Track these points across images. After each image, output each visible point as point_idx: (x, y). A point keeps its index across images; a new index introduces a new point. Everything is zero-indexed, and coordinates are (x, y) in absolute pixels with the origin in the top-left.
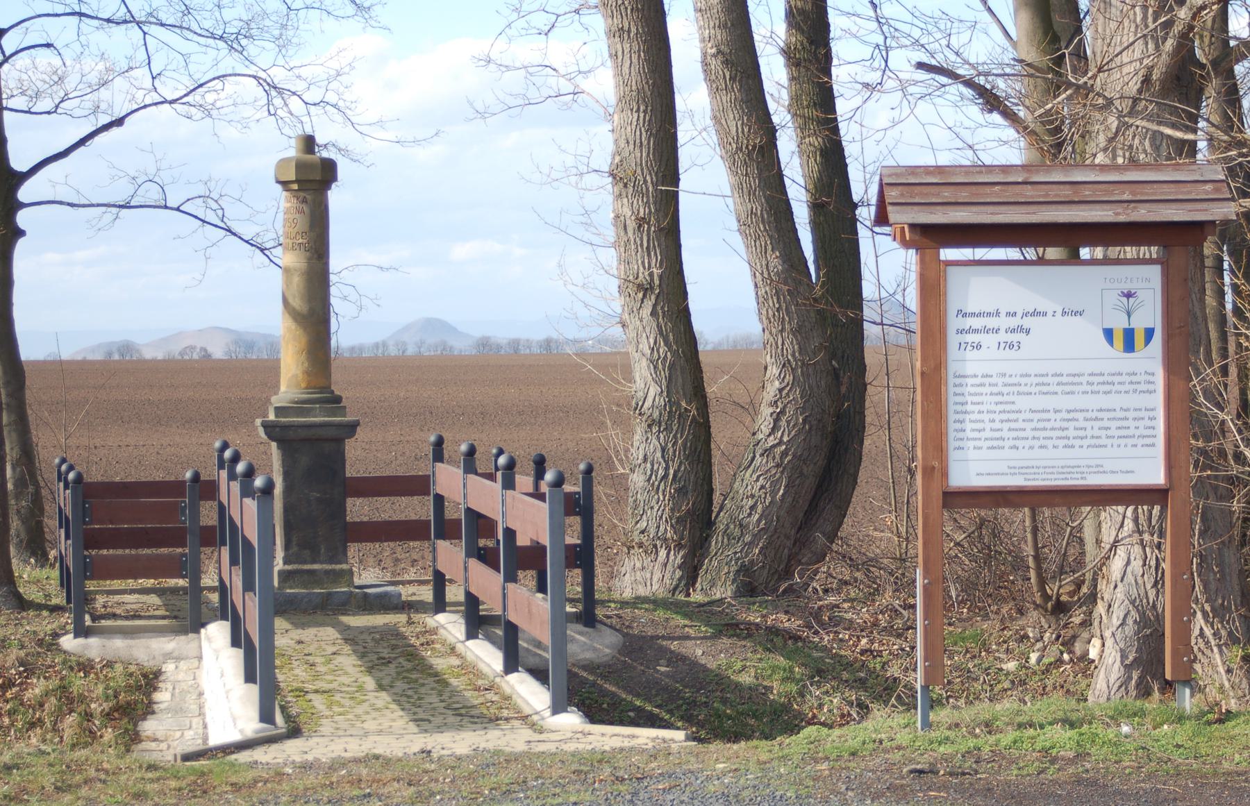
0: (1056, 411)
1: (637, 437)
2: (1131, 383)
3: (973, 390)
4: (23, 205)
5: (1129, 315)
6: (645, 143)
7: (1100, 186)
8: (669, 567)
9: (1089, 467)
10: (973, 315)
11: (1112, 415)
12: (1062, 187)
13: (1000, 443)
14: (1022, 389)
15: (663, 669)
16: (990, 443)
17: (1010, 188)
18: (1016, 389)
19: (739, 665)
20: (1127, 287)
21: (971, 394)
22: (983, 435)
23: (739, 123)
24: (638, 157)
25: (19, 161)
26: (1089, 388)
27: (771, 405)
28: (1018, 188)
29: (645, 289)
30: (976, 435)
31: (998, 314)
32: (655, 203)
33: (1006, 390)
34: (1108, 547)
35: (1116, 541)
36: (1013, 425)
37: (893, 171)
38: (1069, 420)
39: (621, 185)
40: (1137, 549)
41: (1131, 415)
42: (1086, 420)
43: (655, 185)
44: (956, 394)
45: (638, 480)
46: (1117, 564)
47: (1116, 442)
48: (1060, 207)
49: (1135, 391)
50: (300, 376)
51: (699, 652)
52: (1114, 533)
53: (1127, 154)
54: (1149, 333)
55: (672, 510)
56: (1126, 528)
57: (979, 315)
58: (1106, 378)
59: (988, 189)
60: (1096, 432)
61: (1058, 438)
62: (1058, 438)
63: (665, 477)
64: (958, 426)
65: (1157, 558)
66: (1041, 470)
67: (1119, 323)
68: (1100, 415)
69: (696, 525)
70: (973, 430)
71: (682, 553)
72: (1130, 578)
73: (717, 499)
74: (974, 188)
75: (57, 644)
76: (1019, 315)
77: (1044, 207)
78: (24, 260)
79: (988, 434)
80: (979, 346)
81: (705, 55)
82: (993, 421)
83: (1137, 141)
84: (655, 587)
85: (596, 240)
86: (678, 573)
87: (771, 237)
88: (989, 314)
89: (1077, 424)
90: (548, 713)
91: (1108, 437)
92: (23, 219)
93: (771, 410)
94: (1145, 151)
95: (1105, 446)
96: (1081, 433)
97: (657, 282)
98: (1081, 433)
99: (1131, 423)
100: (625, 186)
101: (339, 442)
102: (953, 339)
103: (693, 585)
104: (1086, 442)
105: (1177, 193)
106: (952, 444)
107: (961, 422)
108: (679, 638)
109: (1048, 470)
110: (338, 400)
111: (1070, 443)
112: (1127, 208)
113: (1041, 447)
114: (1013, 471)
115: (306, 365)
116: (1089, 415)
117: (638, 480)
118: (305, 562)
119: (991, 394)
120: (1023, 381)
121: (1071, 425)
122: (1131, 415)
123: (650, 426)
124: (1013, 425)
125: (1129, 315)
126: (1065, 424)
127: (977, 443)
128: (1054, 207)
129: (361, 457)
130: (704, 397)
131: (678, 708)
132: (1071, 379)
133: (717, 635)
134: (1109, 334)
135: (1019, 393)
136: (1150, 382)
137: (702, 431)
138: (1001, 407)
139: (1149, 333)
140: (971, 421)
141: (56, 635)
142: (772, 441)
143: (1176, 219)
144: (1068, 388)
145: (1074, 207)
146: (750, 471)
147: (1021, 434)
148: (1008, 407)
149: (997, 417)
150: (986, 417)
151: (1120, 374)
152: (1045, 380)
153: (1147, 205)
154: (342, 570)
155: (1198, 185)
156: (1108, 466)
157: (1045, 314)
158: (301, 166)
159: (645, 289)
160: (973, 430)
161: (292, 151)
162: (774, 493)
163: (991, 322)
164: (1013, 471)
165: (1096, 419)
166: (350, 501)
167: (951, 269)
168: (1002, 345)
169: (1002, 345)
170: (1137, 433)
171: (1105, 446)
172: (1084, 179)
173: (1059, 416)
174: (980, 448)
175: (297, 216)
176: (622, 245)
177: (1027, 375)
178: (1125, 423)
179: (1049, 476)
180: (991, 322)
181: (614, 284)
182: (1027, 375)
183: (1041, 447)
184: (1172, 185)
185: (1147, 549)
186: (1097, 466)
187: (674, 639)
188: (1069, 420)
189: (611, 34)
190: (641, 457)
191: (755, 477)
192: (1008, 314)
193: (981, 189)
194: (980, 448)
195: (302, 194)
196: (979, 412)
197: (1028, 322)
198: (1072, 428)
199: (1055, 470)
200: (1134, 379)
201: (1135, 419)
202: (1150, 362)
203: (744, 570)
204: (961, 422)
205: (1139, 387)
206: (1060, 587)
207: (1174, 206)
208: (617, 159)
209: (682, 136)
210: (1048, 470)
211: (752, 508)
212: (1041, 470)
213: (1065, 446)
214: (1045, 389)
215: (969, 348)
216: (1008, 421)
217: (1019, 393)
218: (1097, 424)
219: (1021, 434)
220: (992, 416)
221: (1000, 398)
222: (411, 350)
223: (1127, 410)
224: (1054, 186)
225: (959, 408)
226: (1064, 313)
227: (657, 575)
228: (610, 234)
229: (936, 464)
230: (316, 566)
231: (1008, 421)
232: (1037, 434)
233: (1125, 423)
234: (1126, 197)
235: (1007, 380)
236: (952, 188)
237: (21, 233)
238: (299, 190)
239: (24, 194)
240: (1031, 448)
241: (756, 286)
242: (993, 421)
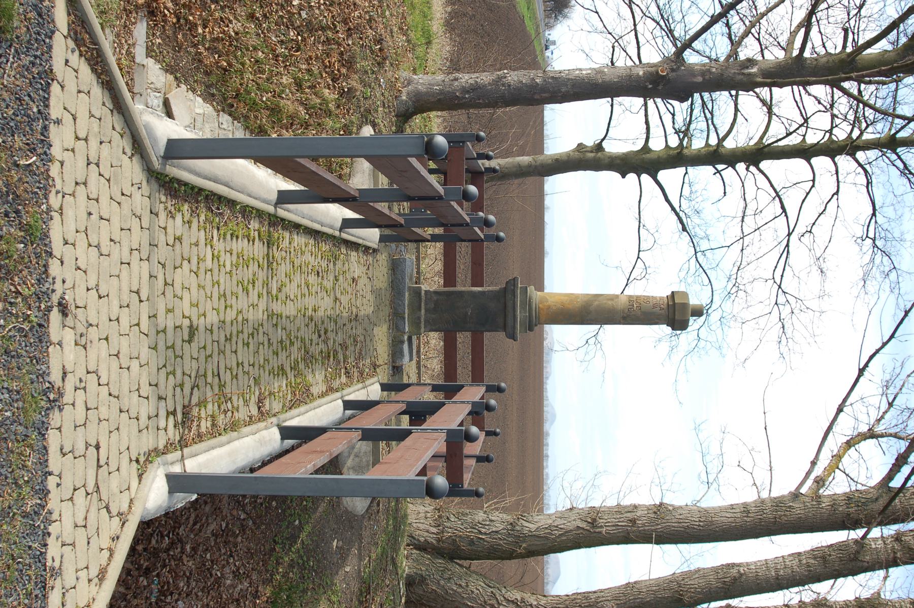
1: (505, 516)
6: (680, 525)
8: (426, 534)
15: (335, 544)
19: (334, 599)
24: (672, 522)
27: (522, 599)
29: (593, 523)
32: (644, 530)
39: (655, 510)
43: (655, 530)
45: (480, 516)
51: (348, 569)
55: (460, 536)
63: (480, 533)
69: (450, 551)
71: (434, 542)
73: (466, 563)
75: (367, 124)
81: (739, 565)
84: (414, 525)
85: (622, 494)
86: (422, 539)
87: (625, 603)
90: (177, 469)
92: (632, 176)
93: (519, 599)
97: (598, 530)
100: (655, 513)
101: (504, 328)
103: (415, 548)
108: (360, 554)
110: (531, 329)
117: (480, 516)
118: (426, 304)
123: (511, 524)
129: (493, 340)
130: (528, 557)
131: (301, 558)
133: (363, 581)
137: (510, 555)
141: (374, 125)
142: (500, 598)
146: (483, 584)
154: (420, 328)
158: (685, 305)
159: (593, 523)
161: (693, 301)
162: (469, 599)
166: (468, 334)
176: (619, 510)
181: (596, 504)
187: (359, 549)
189: (745, 505)
190: (493, 518)
191: (479, 588)
195: (665, 307)
203: (423, 580)
208: (671, 508)
209: (683, 547)
211: (460, 585)
222: (545, 409)
227: (422, 526)
228: (626, 502)
230: (423, 311)
237: (623, 177)
239: (645, 177)
241: (595, 592)
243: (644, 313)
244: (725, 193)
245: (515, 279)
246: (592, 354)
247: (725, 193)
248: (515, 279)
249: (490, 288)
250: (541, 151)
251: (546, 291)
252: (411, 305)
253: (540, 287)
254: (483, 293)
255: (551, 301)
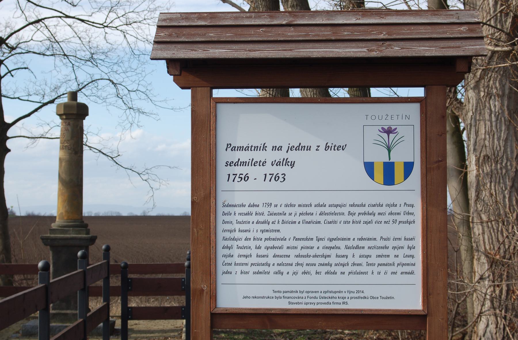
0: (318, 240)
2: (391, 214)
3: (241, 218)
4: (9, 138)
5: (389, 150)
7: (356, 28)
9: (350, 292)
10: (241, 148)
11: (372, 243)
12: (323, 29)
13: (266, 268)
14: (287, 218)
16: (256, 269)
17: (274, 29)
18: (281, 218)
20: (387, 123)
21: (238, 222)
22: (249, 260)
23: (312, 93)
25: (8, 119)
26: (350, 218)
28: (280, 30)
30: (243, 260)
31: (264, 148)
33: (271, 219)
34: (477, 316)
35: (481, 313)
36: (278, 252)
37: (169, 16)
38: (331, 248)
40: (492, 319)
41: (391, 244)
42: (347, 247)
44: (224, 222)
46: (481, 326)
47: (376, 269)
48: (317, 45)
49: (394, 222)
50: (64, 214)
52: (480, 308)
53: (486, 91)
54: (408, 167)
56: (486, 306)
57: (247, 149)
58: (366, 209)
59: (252, 31)
60: (358, 260)
61: (321, 265)
62: (321, 265)
64: (226, 252)
65: (504, 325)
66: (305, 295)
67: (379, 157)
68: (361, 244)
70: (240, 256)
72: (488, 334)
74: (240, 30)
76: (285, 149)
77: (301, 45)
78: (9, 161)
79: (254, 260)
80: (246, 178)
82: (259, 248)
83: (491, 82)
88: (256, 148)
89: (340, 252)
91: (368, 265)
92: (9, 144)
94: (496, 88)
95: (366, 273)
96: (343, 260)
98: (343, 260)
99: (390, 252)
102: (223, 172)
104: (347, 269)
105: (432, 33)
106: (221, 268)
107: (230, 248)
109: (311, 295)
111: (332, 269)
112: (381, 46)
113: (304, 273)
114: (277, 295)
115: (67, 208)
116: (350, 243)
118: (63, 309)
119: (258, 223)
120: (288, 210)
121: (333, 252)
122: (391, 244)
124: (278, 252)
125: (389, 150)
126: (327, 252)
127: (245, 268)
128: (311, 45)
132: (333, 210)
134: (369, 167)
135: (283, 222)
136: (409, 213)
138: (267, 235)
139: (408, 167)
140: (239, 248)
143: (427, 54)
144: (330, 218)
145: (330, 44)
147: (286, 260)
148: (273, 235)
149: (263, 244)
150: (252, 244)
151: (381, 205)
152: (309, 210)
153: (402, 43)
155: (455, 27)
156: (369, 291)
157: (309, 148)
160: (240, 256)
163: (258, 156)
164: (277, 295)
165: (357, 247)
167: (220, 106)
168: (269, 177)
169: (269, 177)
170: (397, 261)
171: (366, 273)
172: (345, 22)
173: (321, 244)
174: (247, 273)
175: (65, 132)
177: (291, 205)
178: (384, 252)
179: (313, 300)
180: (258, 156)
182: (291, 205)
183: (304, 273)
184: (429, 27)
185: (499, 318)
186: (358, 292)
188: (331, 248)
192: (274, 148)
193: (245, 31)
194: (247, 273)
195: (67, 121)
196: (246, 239)
197: (292, 156)
198: (333, 256)
199: (317, 295)
200: (394, 210)
201: (394, 248)
202: (409, 192)
204: (230, 248)
205: (399, 218)
206: (452, 336)
207: (427, 43)
210: (311, 295)
212: (305, 295)
213: (327, 273)
214: (308, 218)
215: (237, 179)
216: (273, 247)
217: (283, 222)
218: (358, 252)
219: (286, 260)
220: (258, 243)
221: (265, 227)
223: (388, 239)
224: (316, 28)
225: (227, 235)
226: (327, 148)
229: (205, 287)
230: (69, 312)
231: (273, 247)
232: (300, 260)
233: (384, 252)
234: (381, 36)
235: (273, 209)
236: (219, 30)
237: (9, 150)
238: (66, 119)
239: (9, 133)
240: (295, 273)
242: (259, 248)
243: (72, 137)
244: (25, 68)
245: (43, 239)
246: (154, 177)
247: (25, 68)
248: (43, 239)
249: (51, 258)
250: (189, 217)
251: (55, 214)
252: (62, 321)
253: (52, 219)
254: (54, 264)
255: (62, 211)
